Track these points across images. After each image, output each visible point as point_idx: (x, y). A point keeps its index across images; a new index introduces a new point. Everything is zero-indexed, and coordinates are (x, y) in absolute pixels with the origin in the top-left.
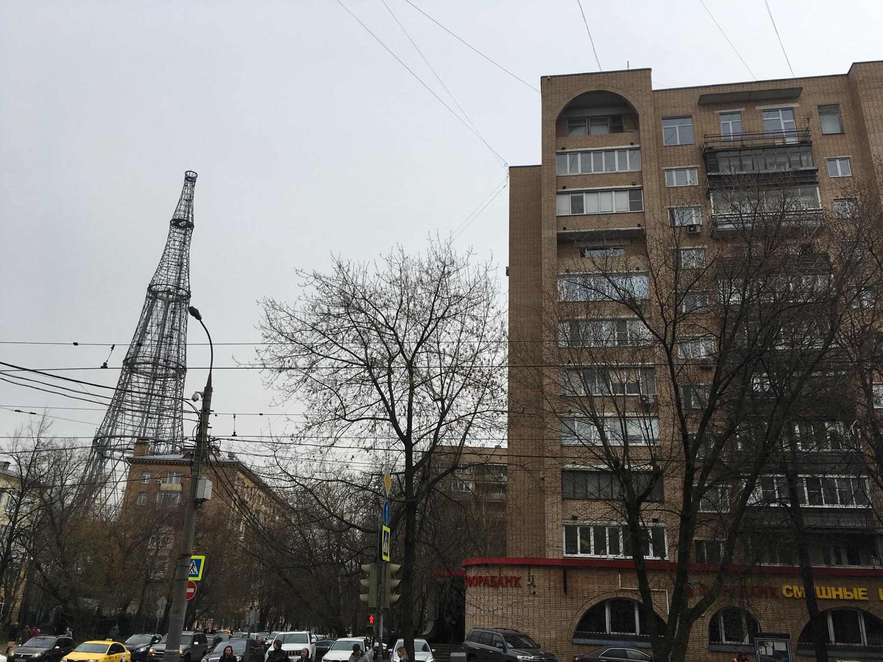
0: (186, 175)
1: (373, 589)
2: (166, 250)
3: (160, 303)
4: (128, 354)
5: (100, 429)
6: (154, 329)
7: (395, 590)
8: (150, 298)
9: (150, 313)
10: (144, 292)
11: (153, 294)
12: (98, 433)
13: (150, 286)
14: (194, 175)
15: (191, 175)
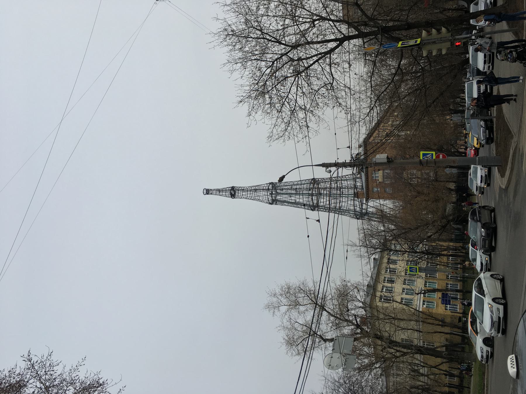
0: (206, 194)
1: (438, 46)
2: (249, 199)
3: (278, 197)
4: (308, 209)
5: (351, 217)
6: (293, 198)
7: (439, 31)
8: (276, 203)
9: (285, 202)
10: (274, 206)
11: (274, 202)
12: (354, 218)
13: (270, 204)
14: (205, 190)
15: (205, 192)
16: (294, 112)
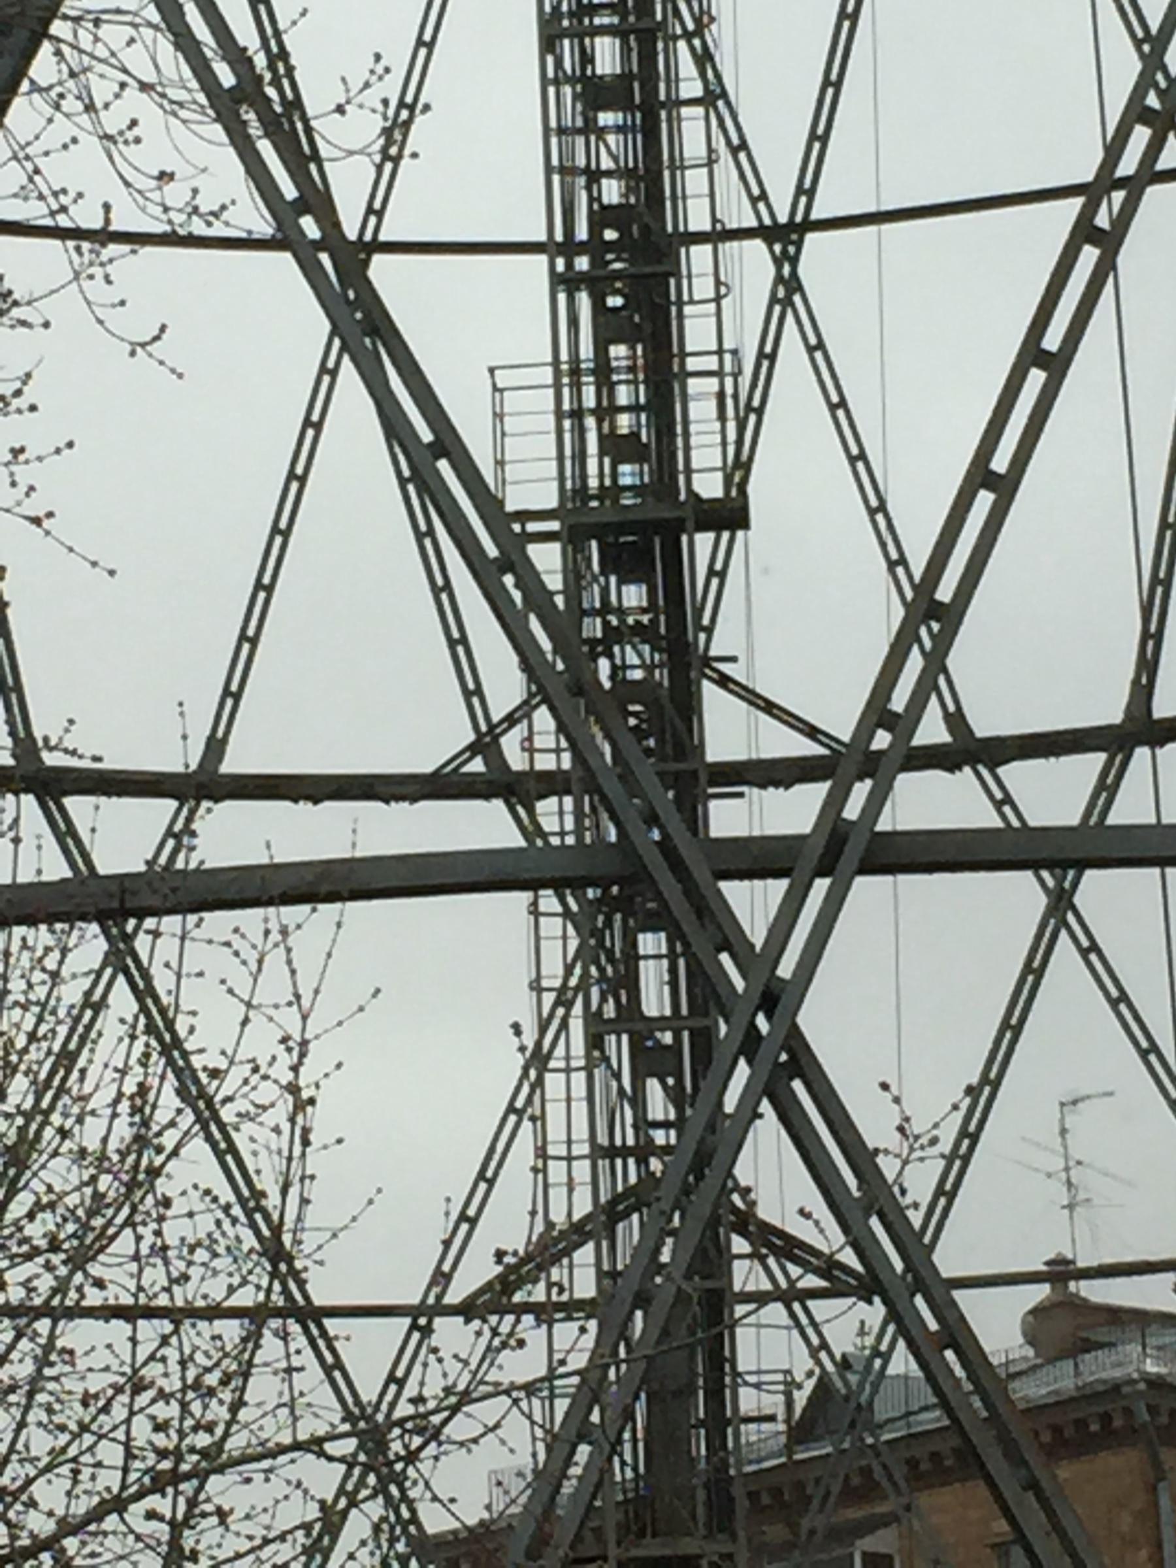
16: (354, 1425)
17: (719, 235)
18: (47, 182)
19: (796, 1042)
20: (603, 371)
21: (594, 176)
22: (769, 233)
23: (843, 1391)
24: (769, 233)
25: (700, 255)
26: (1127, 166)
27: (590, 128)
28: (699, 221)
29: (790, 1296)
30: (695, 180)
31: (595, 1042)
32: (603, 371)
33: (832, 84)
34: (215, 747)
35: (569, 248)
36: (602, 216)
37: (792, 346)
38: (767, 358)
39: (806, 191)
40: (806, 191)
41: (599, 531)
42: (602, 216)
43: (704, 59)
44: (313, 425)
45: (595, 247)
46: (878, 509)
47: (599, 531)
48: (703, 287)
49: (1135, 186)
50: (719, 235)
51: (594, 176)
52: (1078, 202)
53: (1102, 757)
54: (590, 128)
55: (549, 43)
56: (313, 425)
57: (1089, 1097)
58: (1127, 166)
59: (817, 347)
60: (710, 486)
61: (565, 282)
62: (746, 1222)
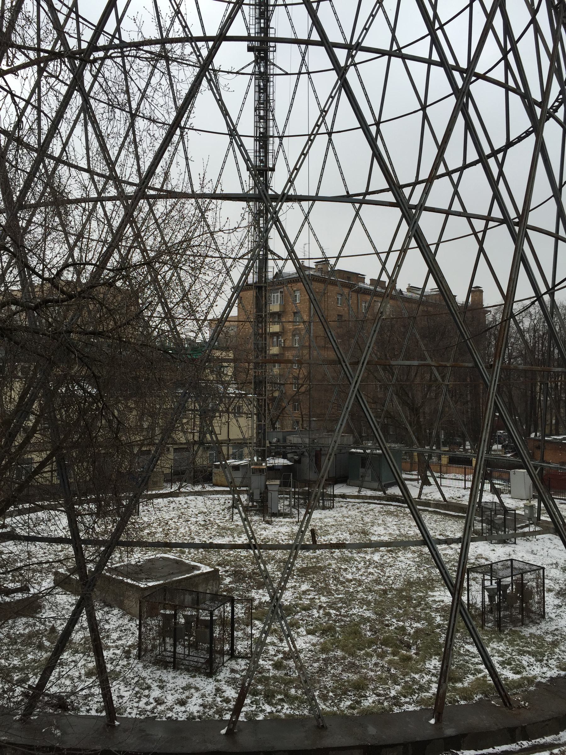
17: (273, 137)
18: (384, 145)
19: (278, 218)
20: (260, 152)
21: (260, 128)
22: (279, 137)
23: (141, 48)
24: (279, 137)
25: (271, 139)
26: (314, 132)
27: (259, 122)
28: (271, 134)
29: (274, 259)
30: (271, 129)
31: (255, 229)
32: (260, 152)
33: (295, 93)
34: (317, 194)
35: (256, 137)
36: (260, 133)
37: (281, 151)
38: (278, 152)
39: (284, 132)
40: (284, 132)
41: (258, 170)
42: (260, 133)
43: (273, 115)
44: (226, 156)
45: (260, 136)
46: (287, 165)
47: (258, 170)
48: (271, 142)
49: (315, 135)
50: (273, 137)
51: (260, 128)
52: (510, 93)
53: (227, 35)
54: (259, 122)
55: (255, 111)
56: (226, 156)
57: (321, 247)
58: (314, 132)
59: (284, 151)
60: (271, 166)
61: (256, 140)
62: (270, 250)
